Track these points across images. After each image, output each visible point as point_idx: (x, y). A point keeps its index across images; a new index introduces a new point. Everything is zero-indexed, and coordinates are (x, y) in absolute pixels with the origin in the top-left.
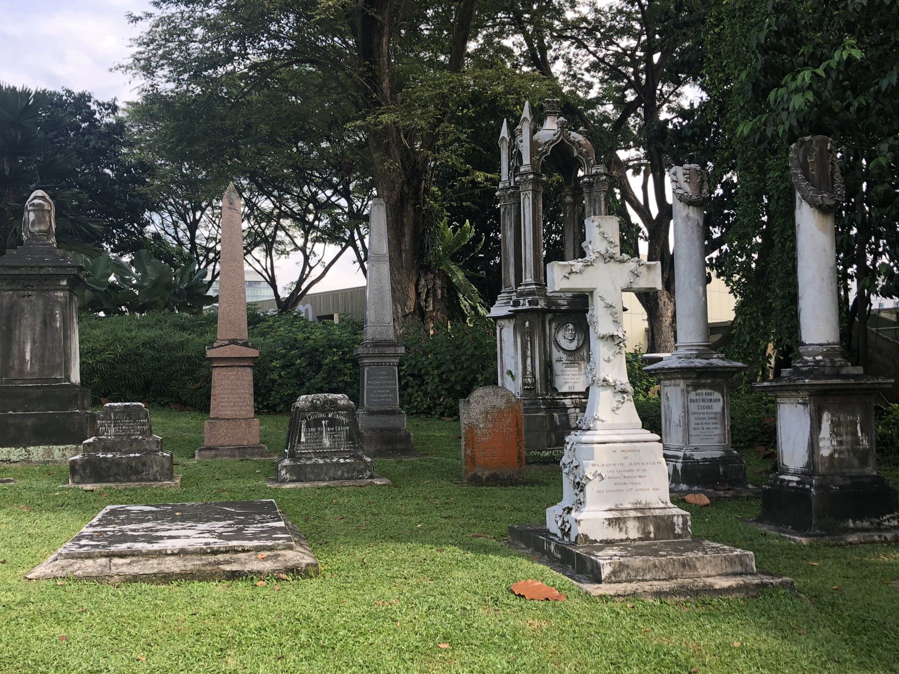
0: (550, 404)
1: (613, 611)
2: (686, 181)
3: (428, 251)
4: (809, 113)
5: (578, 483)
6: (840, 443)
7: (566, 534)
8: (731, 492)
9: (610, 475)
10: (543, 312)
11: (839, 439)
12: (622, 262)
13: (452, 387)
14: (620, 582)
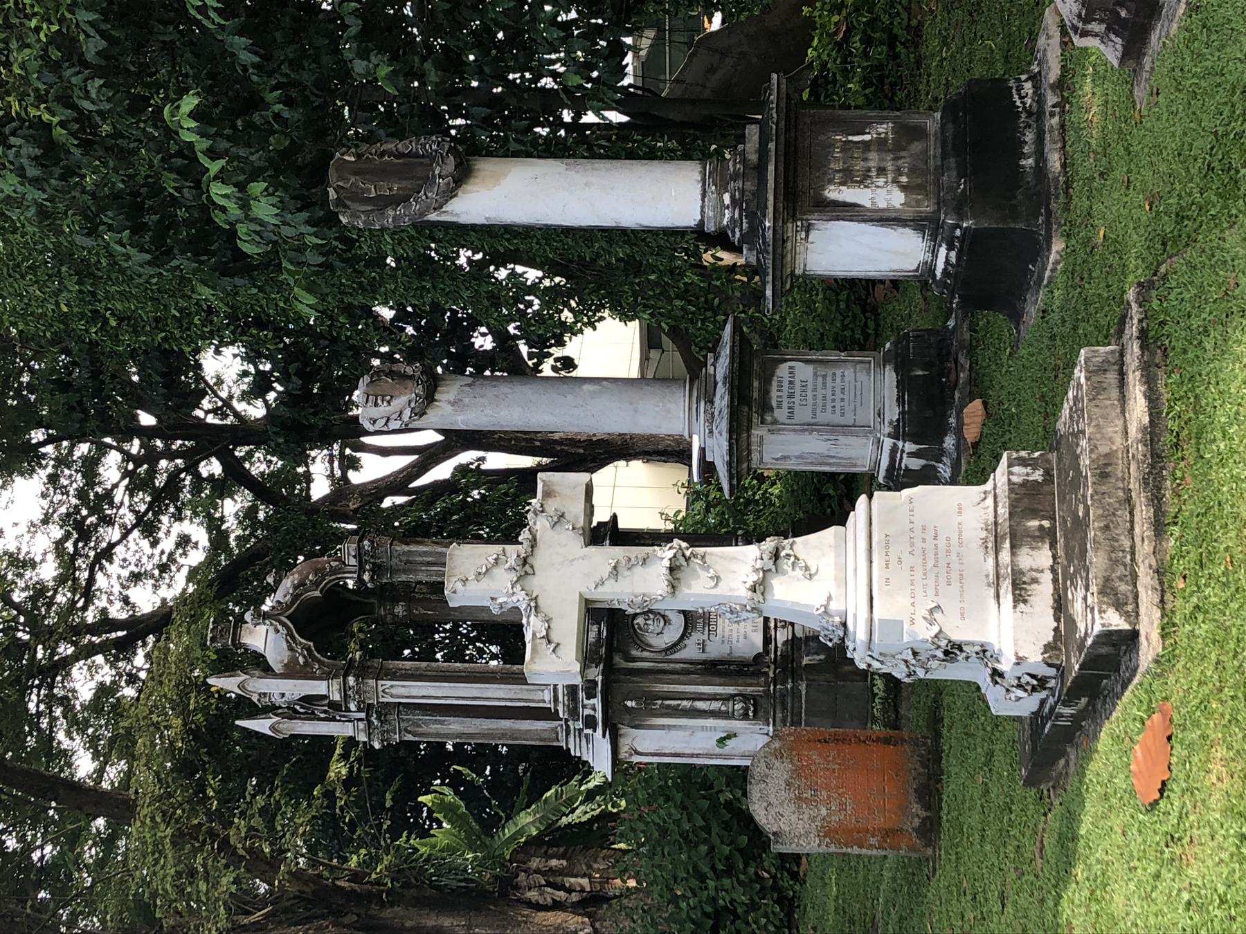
0: (784, 670)
1: (1192, 617)
2: (389, 402)
3: (472, 881)
4: (286, 188)
5: (946, 653)
6: (881, 171)
7: (1042, 682)
8: (962, 359)
9: (931, 592)
10: (610, 672)
11: (874, 174)
12: (534, 543)
13: (740, 851)
14: (1136, 597)
